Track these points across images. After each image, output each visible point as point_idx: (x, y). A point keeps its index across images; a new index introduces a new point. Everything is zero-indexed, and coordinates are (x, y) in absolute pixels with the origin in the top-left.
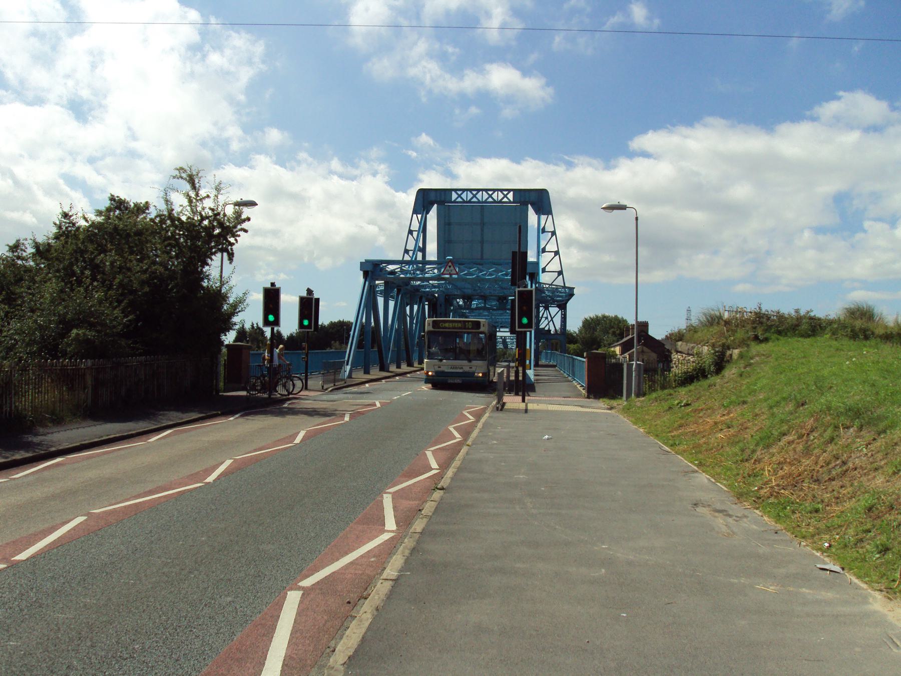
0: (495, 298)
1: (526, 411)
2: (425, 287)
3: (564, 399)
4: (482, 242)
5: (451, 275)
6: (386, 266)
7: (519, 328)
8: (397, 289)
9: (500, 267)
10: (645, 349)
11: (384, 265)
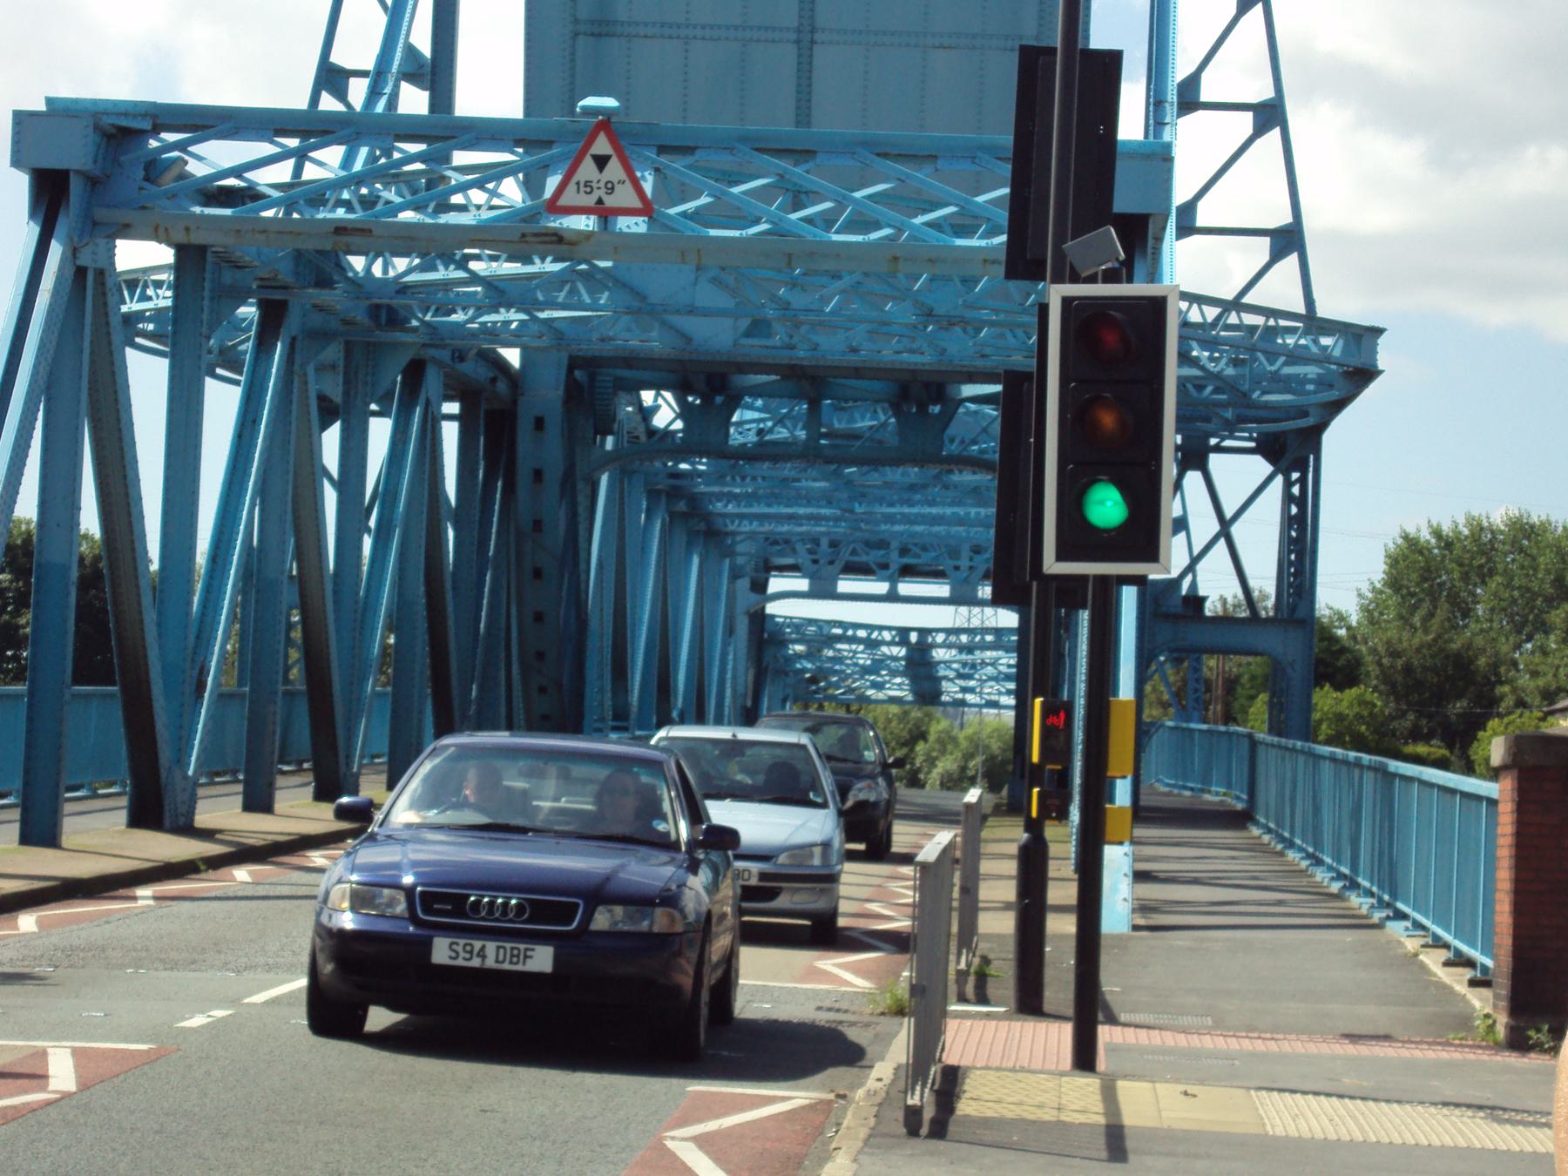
0: (877, 386)
1: (1116, 1141)
2: (440, 297)
3: (1350, 1049)
4: (806, 38)
5: (605, 214)
6: (182, 146)
7: (1061, 556)
8: (264, 306)
9: (920, 176)
11: (171, 137)
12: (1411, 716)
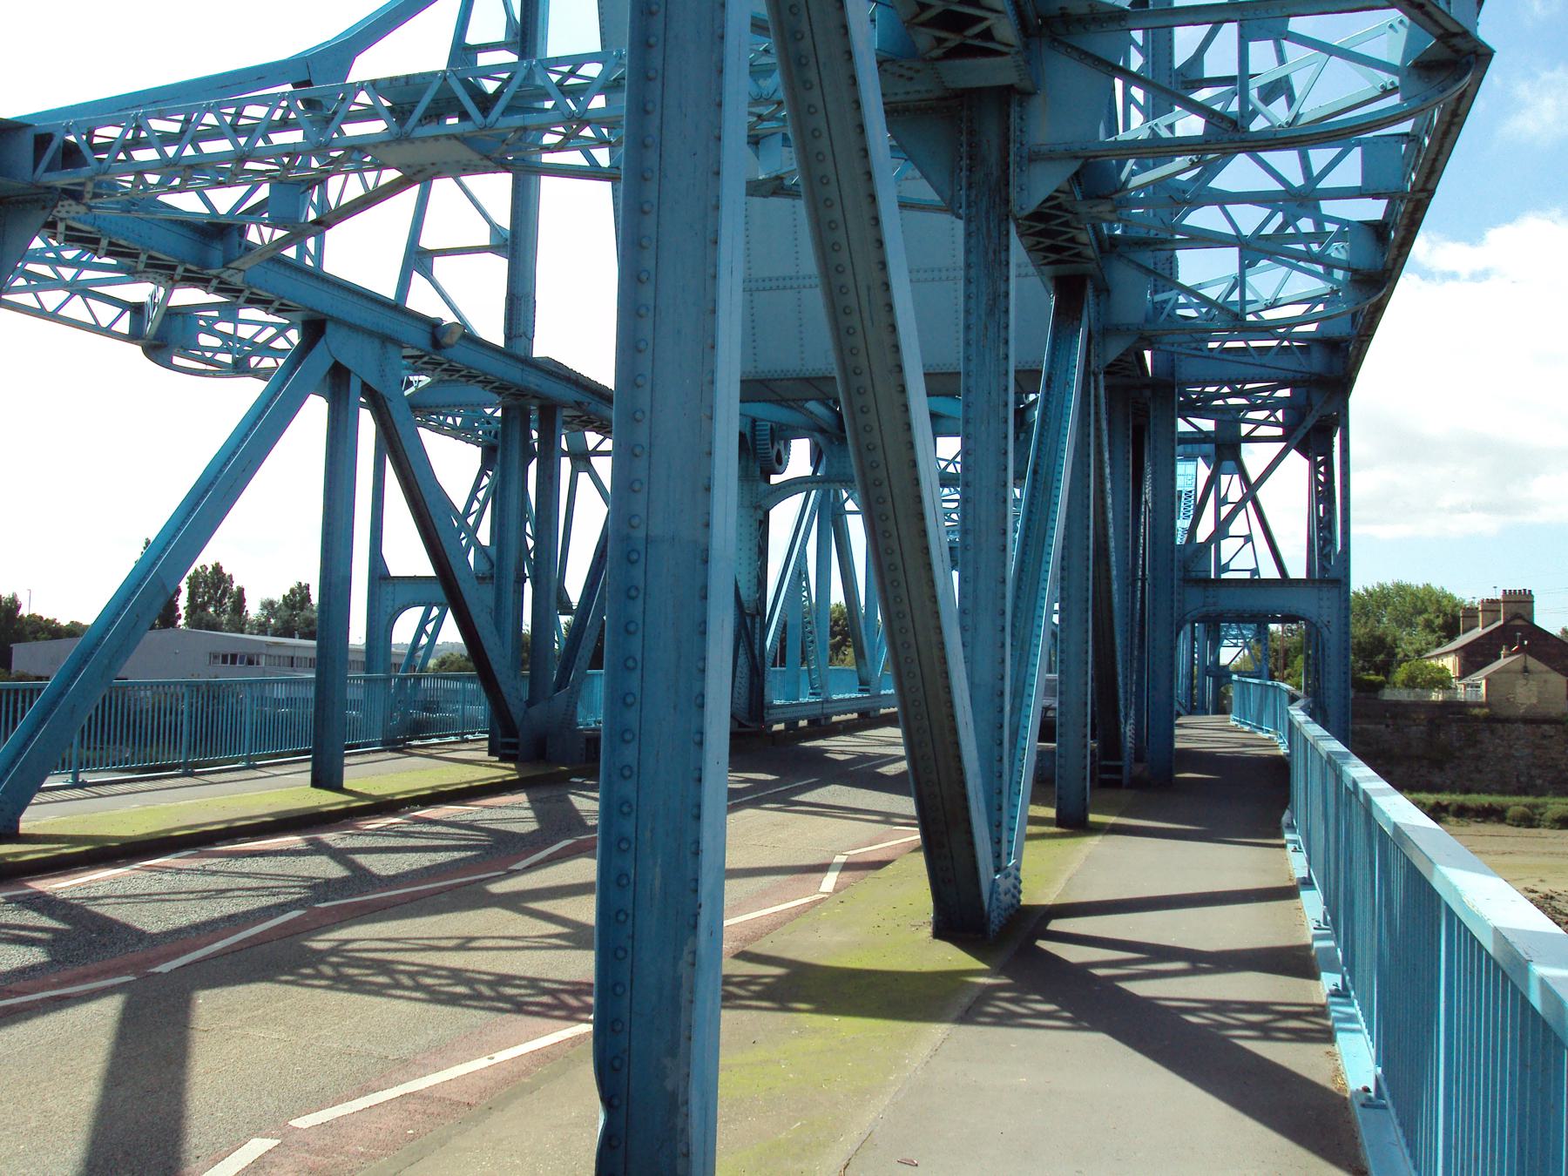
10: (1533, 663)
12: (1361, 662)
